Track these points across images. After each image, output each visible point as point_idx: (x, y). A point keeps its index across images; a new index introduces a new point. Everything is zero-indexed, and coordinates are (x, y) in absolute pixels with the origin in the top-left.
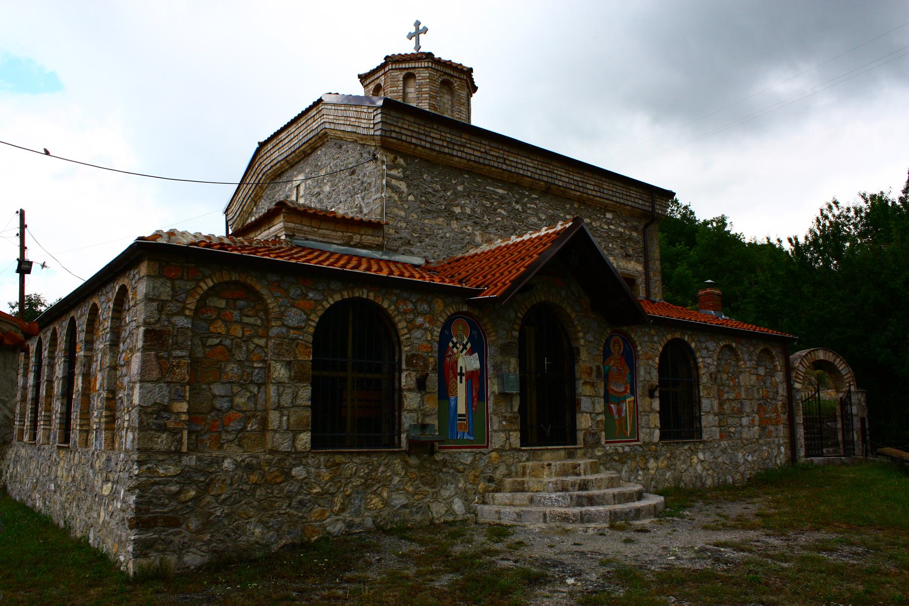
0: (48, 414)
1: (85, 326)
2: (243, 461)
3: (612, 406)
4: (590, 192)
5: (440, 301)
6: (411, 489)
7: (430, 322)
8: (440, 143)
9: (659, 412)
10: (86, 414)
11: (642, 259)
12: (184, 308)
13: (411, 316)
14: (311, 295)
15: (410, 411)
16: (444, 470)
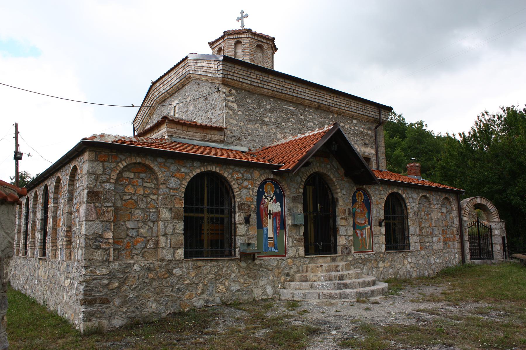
0: (33, 240)
2: (145, 266)
4: (343, 108)
5: (257, 172)
6: (242, 281)
7: (252, 184)
8: (256, 81)
9: (385, 235)
10: (55, 240)
12: (110, 178)
13: (240, 181)
14: (183, 170)
15: (241, 236)
16: (261, 269)
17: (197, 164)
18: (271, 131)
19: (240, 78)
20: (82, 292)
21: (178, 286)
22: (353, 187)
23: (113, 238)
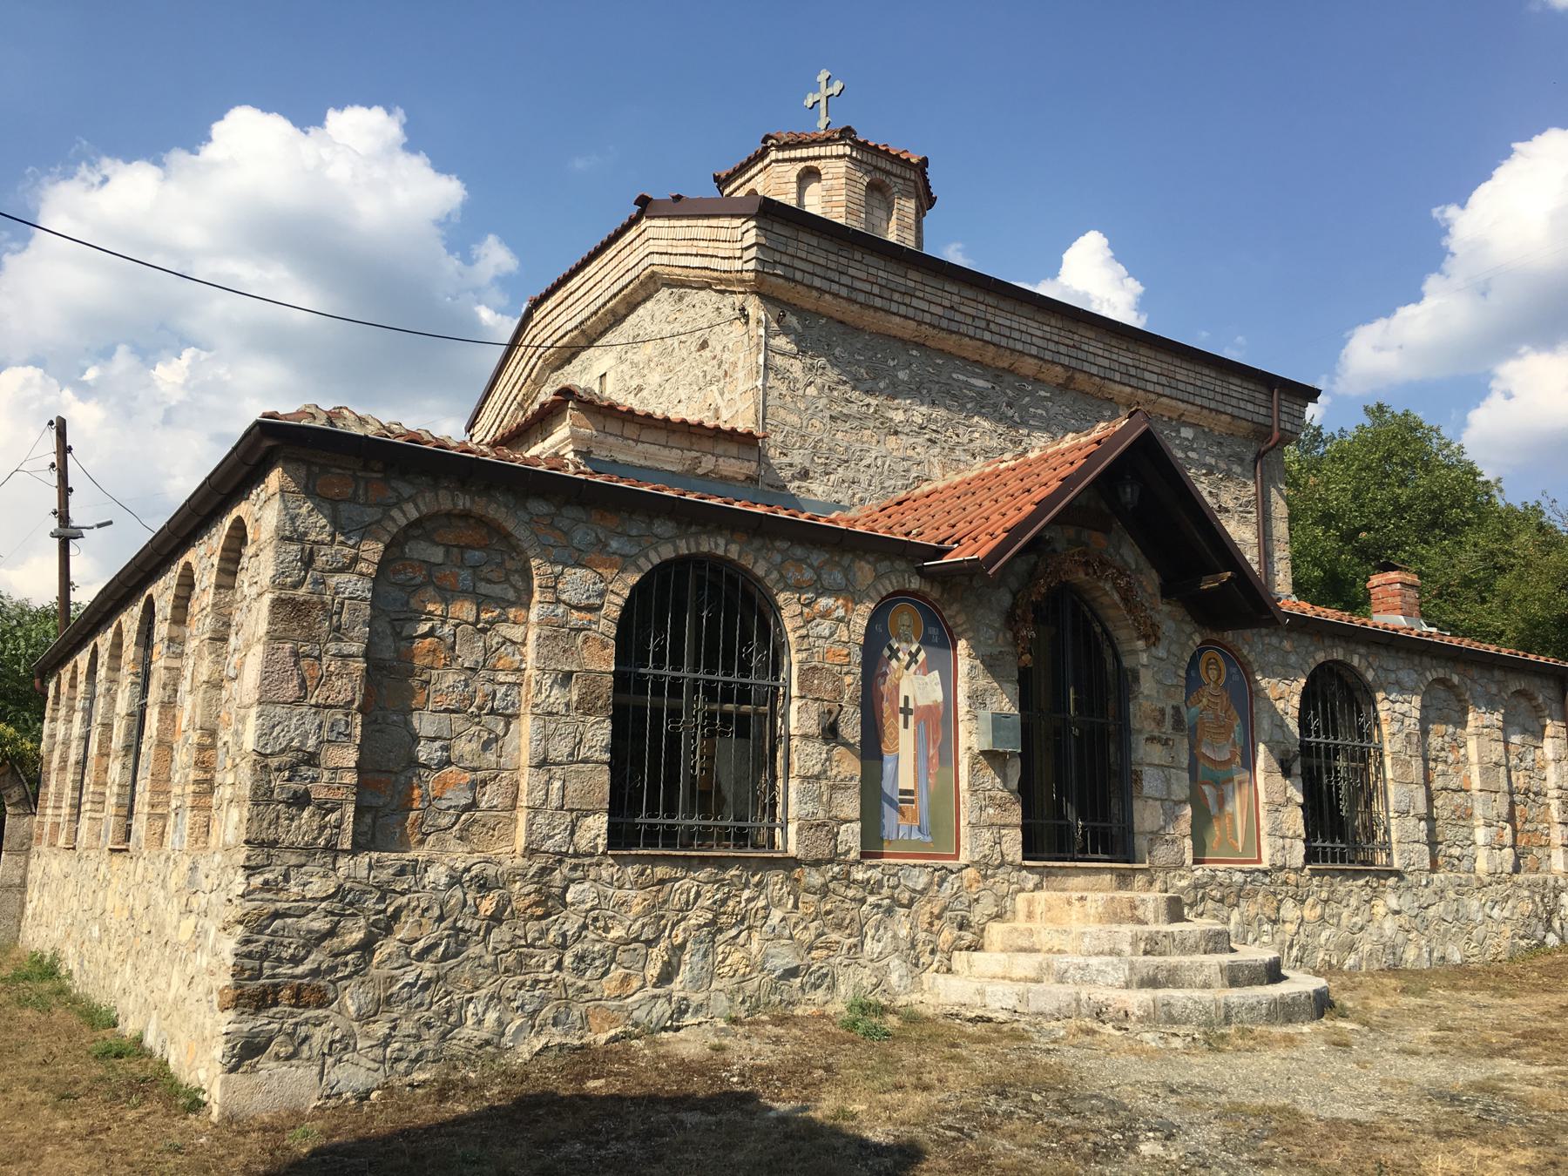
0: (99, 789)
1: (169, 610)
2: (468, 870)
3: (1206, 788)
4: (1150, 387)
5: (867, 567)
8: (867, 287)
9: (1302, 806)
10: (161, 784)
11: (1253, 517)
12: (355, 560)
14: (614, 544)
17: (663, 528)
18: (910, 452)
19: (813, 274)
20: (230, 961)
21: (578, 948)
22: (1190, 637)
23: (360, 767)
